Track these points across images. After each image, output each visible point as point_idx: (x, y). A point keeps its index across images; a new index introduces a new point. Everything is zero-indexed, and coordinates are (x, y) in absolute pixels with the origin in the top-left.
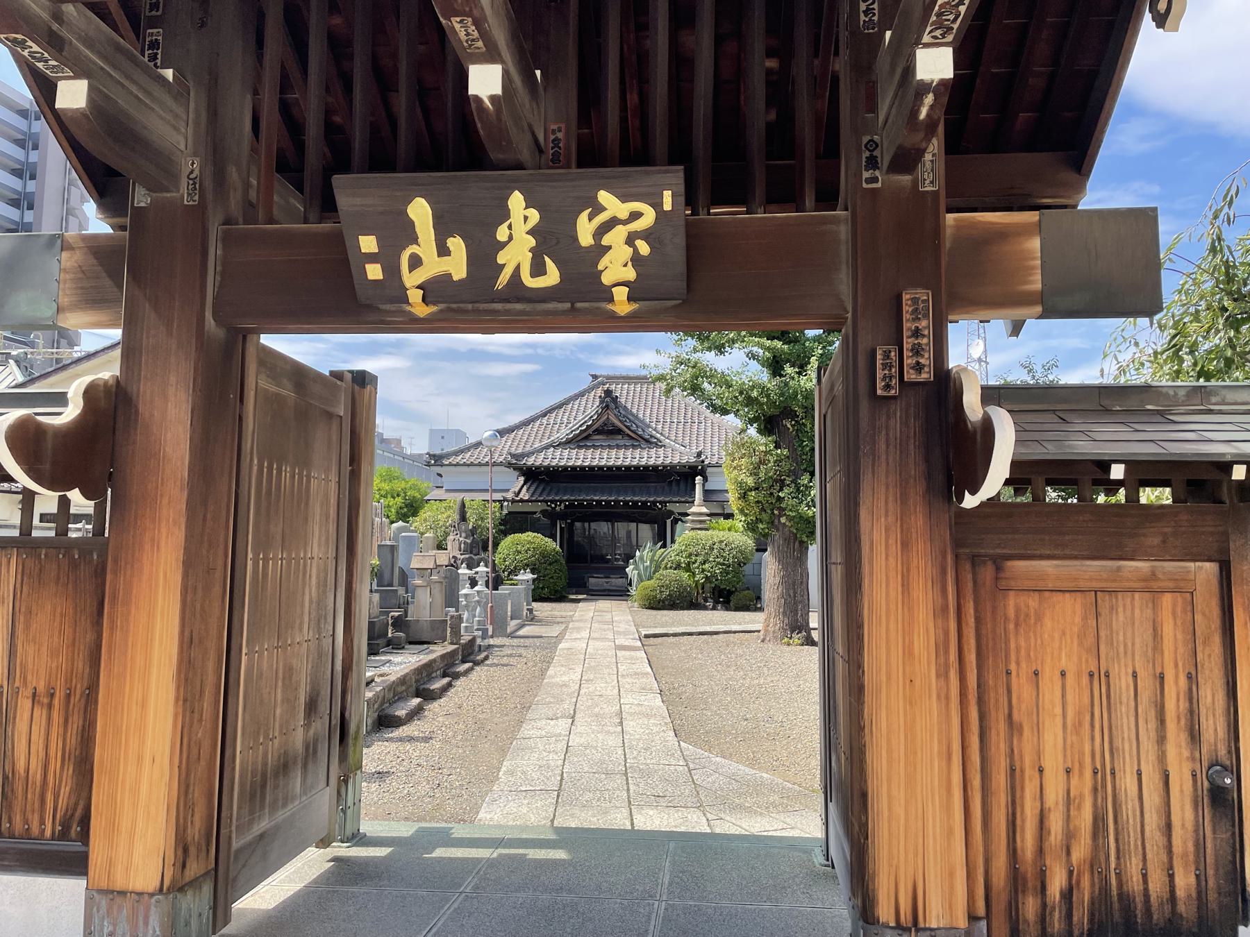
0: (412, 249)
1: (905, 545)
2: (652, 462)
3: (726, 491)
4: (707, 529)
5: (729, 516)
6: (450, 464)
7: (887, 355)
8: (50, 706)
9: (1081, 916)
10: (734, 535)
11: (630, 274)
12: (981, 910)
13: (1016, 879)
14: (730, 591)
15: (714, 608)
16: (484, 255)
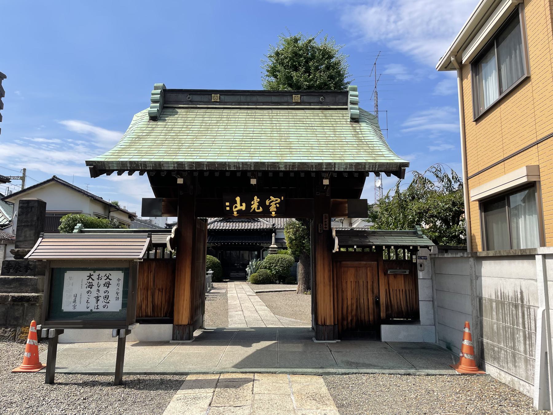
1: (324, 259)
2: (255, 228)
3: (284, 239)
4: (276, 254)
5: (286, 248)
9: (354, 324)
10: (287, 255)
12: (336, 323)
13: (343, 319)
14: (285, 276)
15: (279, 283)
16: (249, 206)
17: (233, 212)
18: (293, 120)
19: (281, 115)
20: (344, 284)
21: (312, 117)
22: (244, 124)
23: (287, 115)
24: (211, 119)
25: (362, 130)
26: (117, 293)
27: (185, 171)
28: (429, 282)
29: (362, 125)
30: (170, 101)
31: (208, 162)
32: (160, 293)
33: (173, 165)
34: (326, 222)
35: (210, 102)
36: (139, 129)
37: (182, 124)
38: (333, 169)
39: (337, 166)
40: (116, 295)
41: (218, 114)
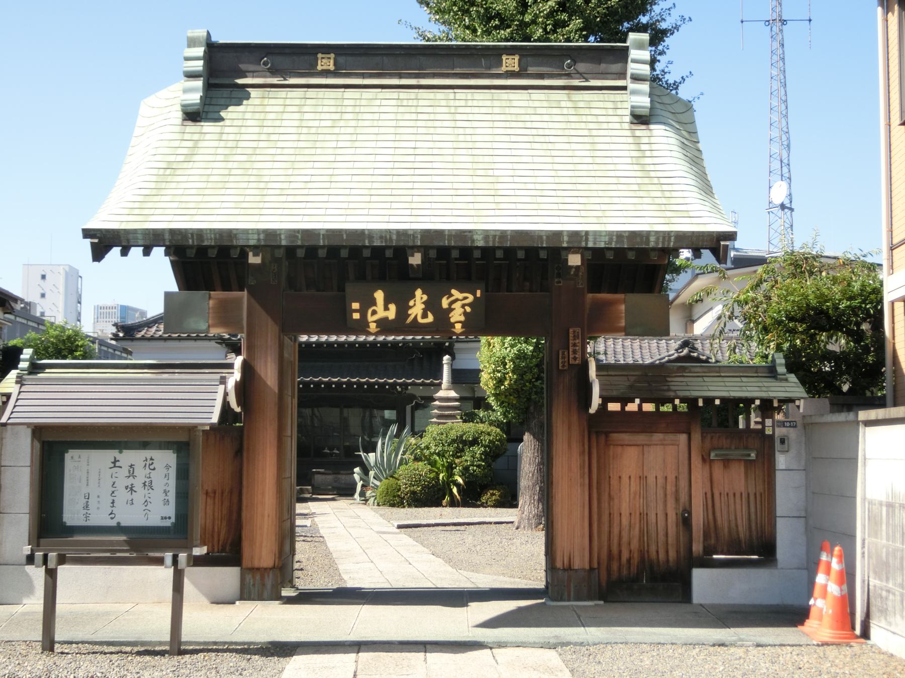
0: (374, 308)
6: (143, 338)
7: (563, 354)
8: (214, 498)
11: (462, 318)
12: (596, 566)
16: (403, 311)
17: (367, 324)
18: (502, 117)
19: (475, 103)
20: (614, 482)
21: (544, 111)
22: (392, 130)
23: (488, 103)
24: (318, 116)
25: (654, 147)
26: (166, 492)
27: (279, 247)
28: (798, 478)
29: (655, 133)
30: (226, 73)
31: (328, 230)
32: (210, 501)
33: (256, 237)
34: (575, 345)
35: (313, 72)
36: (166, 144)
37: (257, 130)
38: (583, 244)
39: (591, 238)
40: (163, 496)
41: (333, 102)
